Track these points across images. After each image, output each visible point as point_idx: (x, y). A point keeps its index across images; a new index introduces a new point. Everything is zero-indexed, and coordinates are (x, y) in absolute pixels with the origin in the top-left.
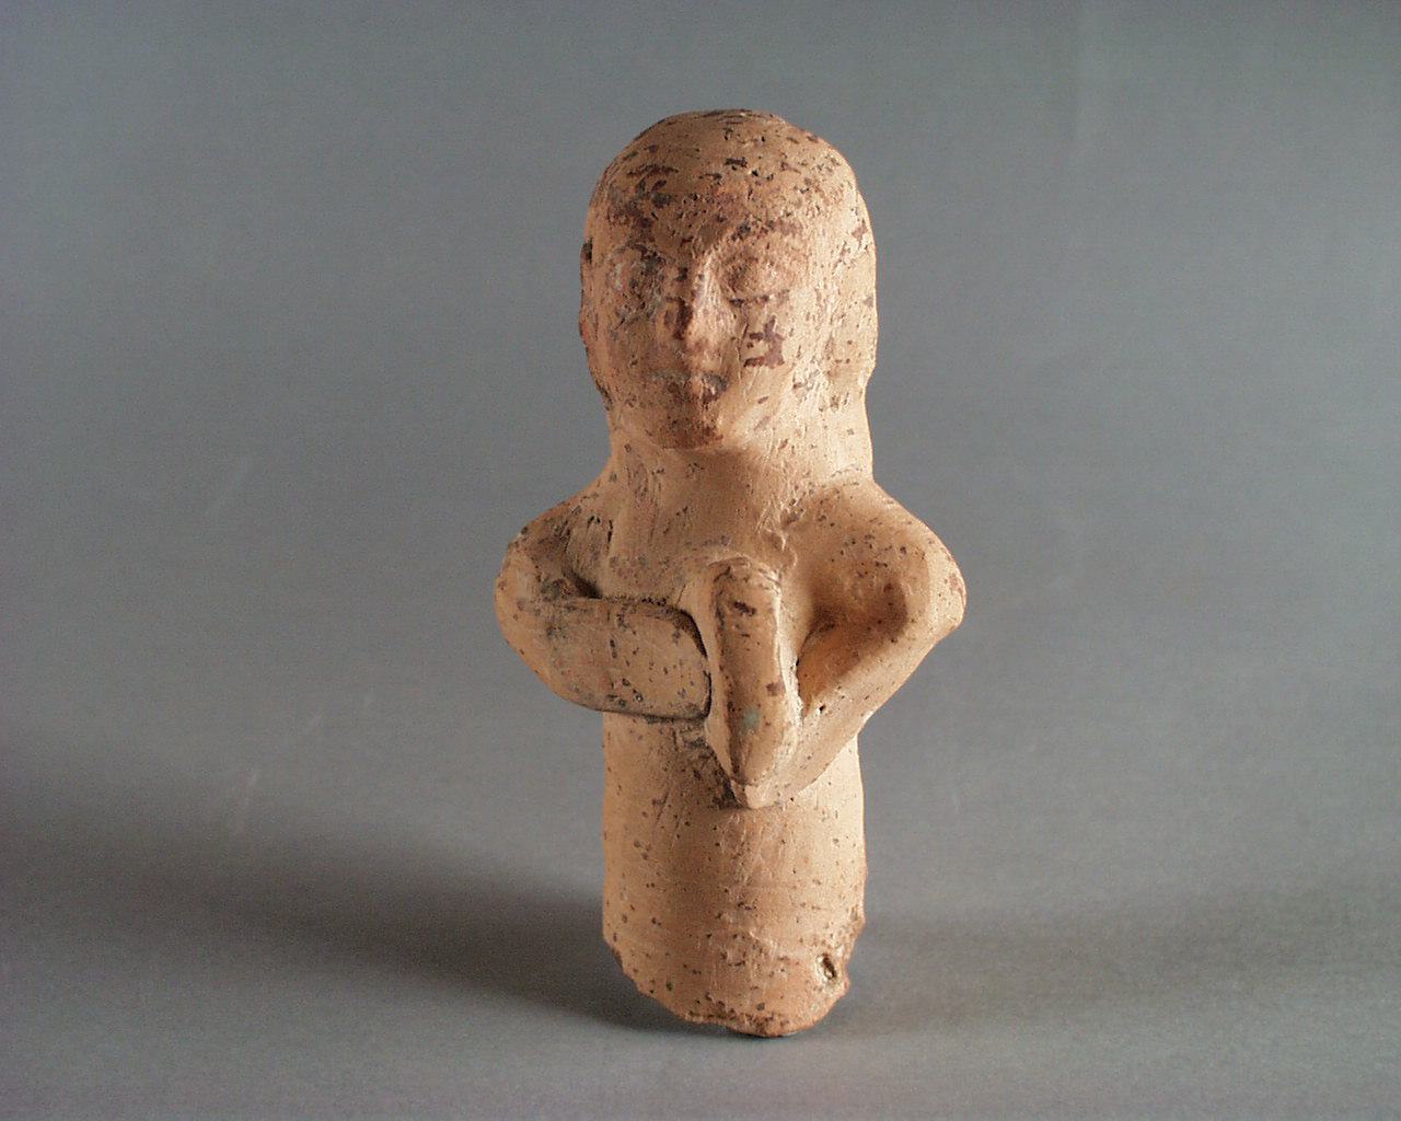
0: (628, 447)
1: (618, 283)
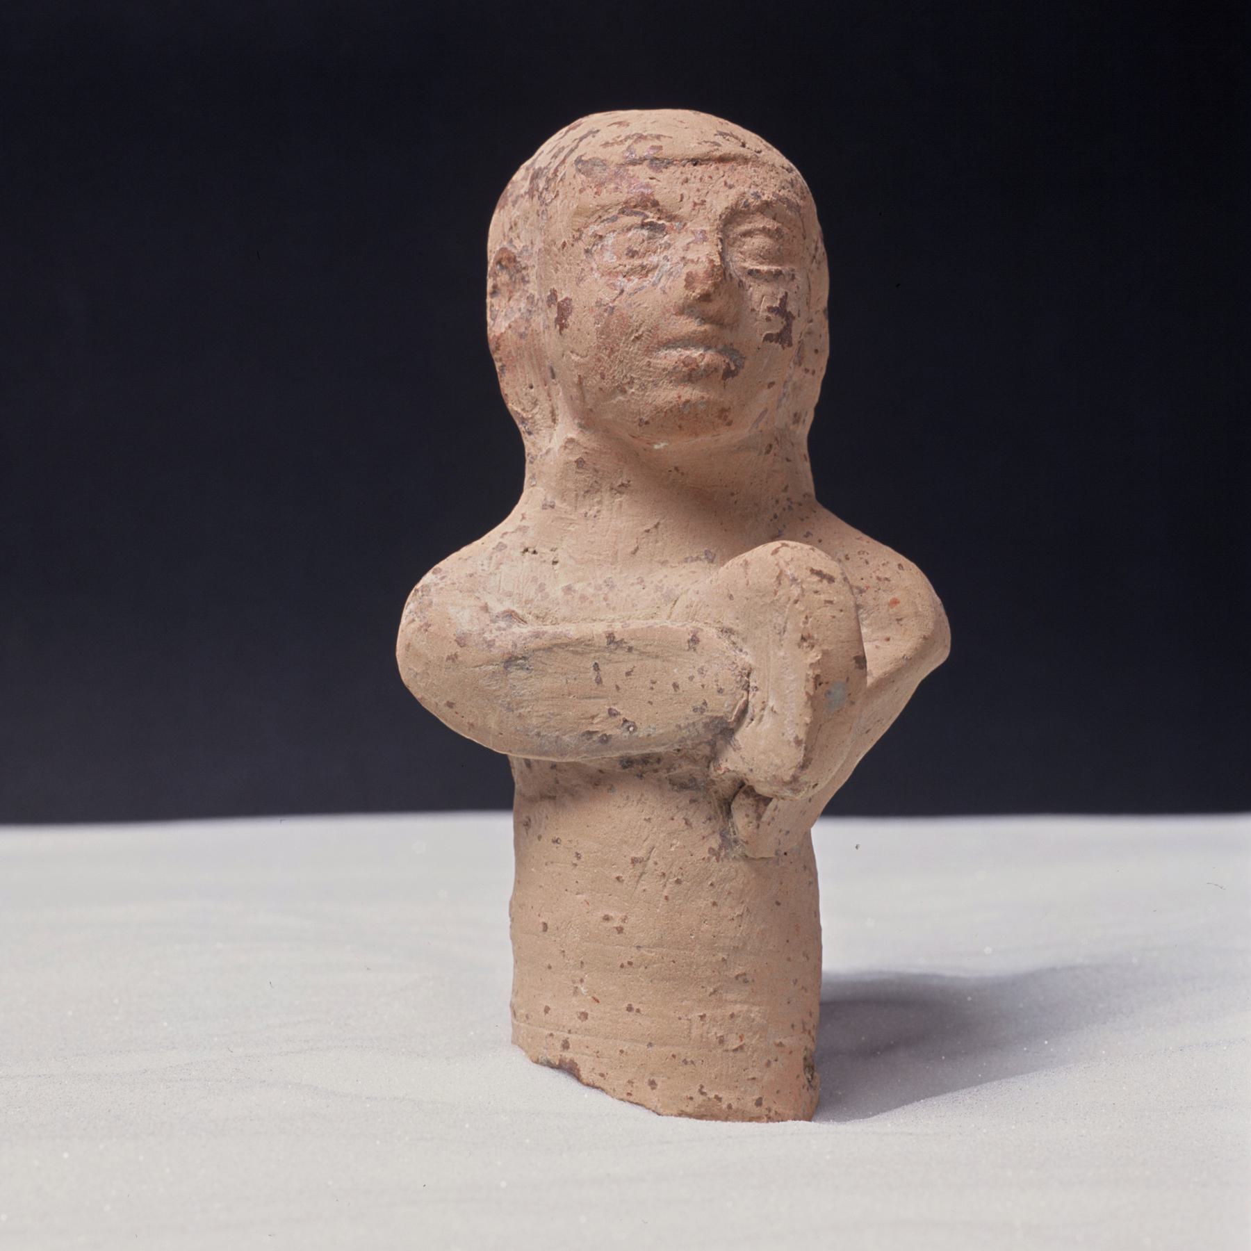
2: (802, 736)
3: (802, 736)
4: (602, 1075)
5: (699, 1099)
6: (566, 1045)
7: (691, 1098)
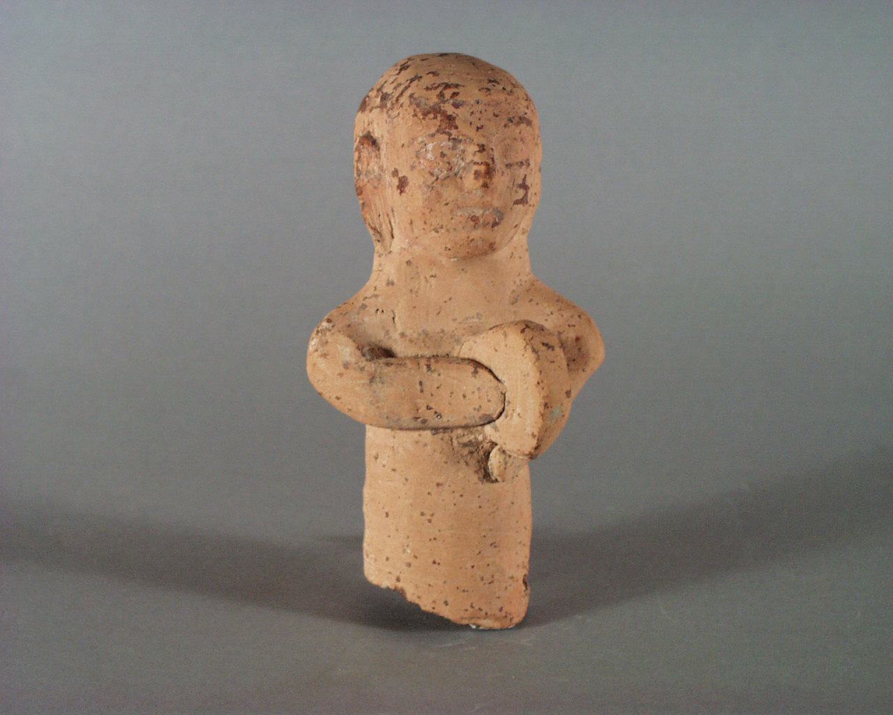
0: (409, 263)
1: (429, 156)
2: (536, 433)
3: (536, 433)
4: (419, 597)
5: (470, 610)
6: (398, 580)
7: (467, 610)
